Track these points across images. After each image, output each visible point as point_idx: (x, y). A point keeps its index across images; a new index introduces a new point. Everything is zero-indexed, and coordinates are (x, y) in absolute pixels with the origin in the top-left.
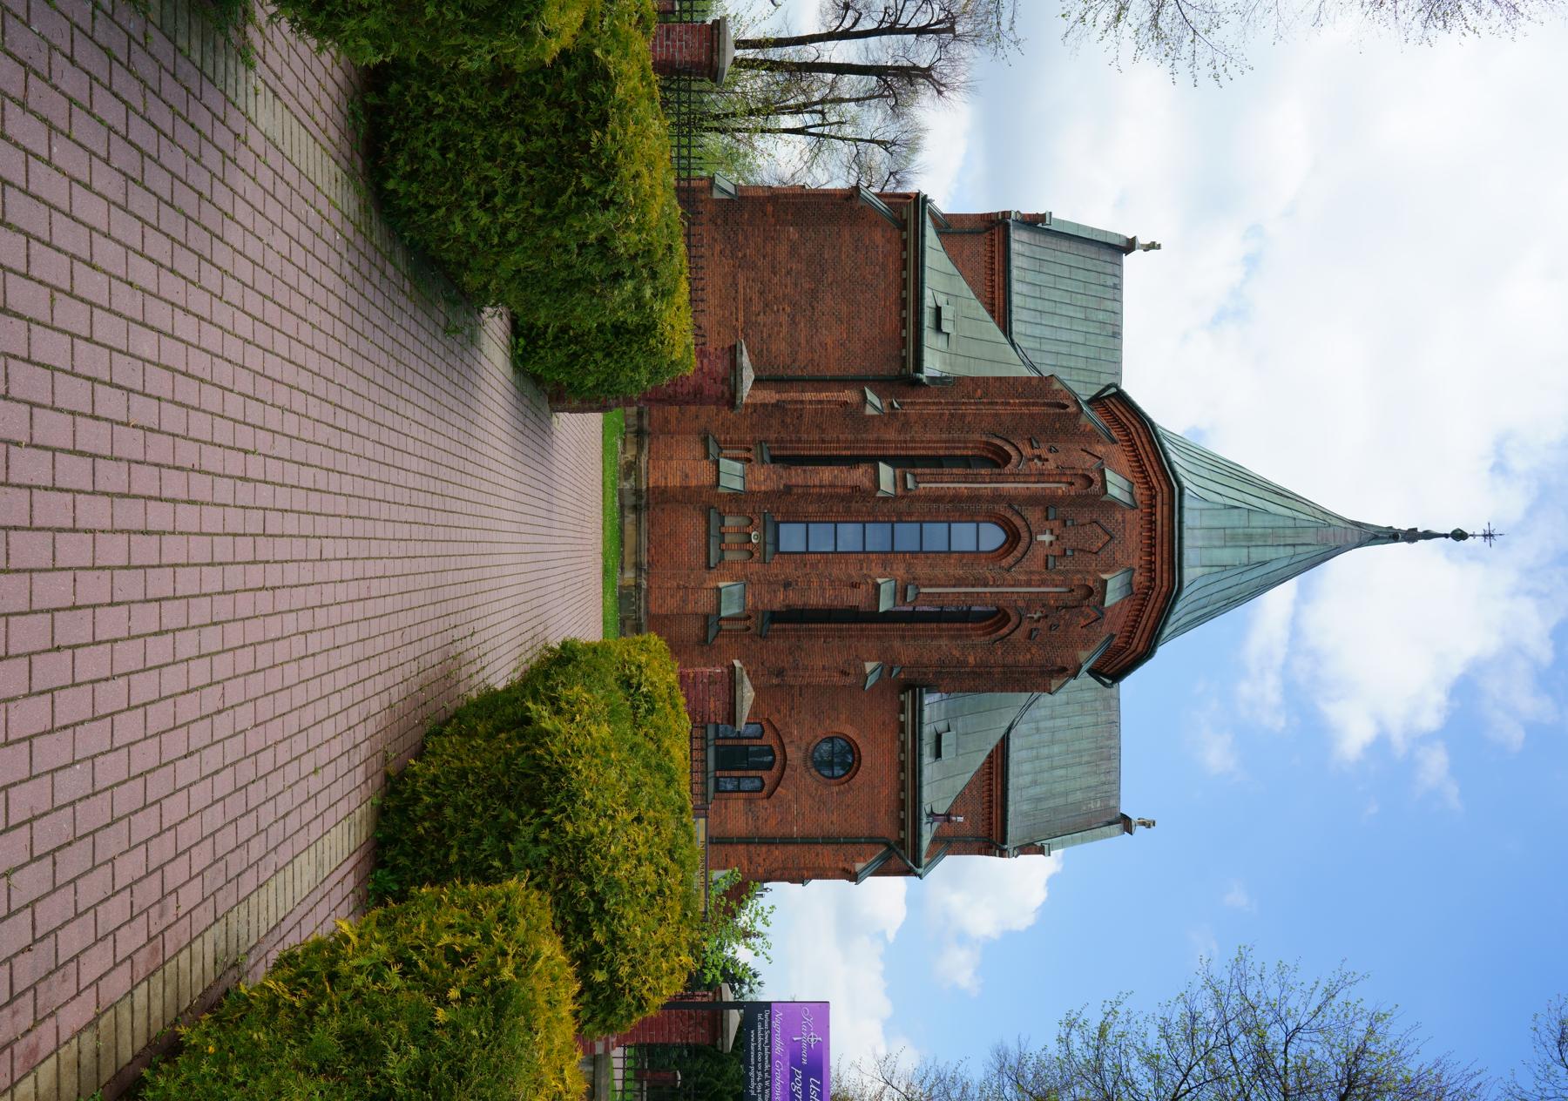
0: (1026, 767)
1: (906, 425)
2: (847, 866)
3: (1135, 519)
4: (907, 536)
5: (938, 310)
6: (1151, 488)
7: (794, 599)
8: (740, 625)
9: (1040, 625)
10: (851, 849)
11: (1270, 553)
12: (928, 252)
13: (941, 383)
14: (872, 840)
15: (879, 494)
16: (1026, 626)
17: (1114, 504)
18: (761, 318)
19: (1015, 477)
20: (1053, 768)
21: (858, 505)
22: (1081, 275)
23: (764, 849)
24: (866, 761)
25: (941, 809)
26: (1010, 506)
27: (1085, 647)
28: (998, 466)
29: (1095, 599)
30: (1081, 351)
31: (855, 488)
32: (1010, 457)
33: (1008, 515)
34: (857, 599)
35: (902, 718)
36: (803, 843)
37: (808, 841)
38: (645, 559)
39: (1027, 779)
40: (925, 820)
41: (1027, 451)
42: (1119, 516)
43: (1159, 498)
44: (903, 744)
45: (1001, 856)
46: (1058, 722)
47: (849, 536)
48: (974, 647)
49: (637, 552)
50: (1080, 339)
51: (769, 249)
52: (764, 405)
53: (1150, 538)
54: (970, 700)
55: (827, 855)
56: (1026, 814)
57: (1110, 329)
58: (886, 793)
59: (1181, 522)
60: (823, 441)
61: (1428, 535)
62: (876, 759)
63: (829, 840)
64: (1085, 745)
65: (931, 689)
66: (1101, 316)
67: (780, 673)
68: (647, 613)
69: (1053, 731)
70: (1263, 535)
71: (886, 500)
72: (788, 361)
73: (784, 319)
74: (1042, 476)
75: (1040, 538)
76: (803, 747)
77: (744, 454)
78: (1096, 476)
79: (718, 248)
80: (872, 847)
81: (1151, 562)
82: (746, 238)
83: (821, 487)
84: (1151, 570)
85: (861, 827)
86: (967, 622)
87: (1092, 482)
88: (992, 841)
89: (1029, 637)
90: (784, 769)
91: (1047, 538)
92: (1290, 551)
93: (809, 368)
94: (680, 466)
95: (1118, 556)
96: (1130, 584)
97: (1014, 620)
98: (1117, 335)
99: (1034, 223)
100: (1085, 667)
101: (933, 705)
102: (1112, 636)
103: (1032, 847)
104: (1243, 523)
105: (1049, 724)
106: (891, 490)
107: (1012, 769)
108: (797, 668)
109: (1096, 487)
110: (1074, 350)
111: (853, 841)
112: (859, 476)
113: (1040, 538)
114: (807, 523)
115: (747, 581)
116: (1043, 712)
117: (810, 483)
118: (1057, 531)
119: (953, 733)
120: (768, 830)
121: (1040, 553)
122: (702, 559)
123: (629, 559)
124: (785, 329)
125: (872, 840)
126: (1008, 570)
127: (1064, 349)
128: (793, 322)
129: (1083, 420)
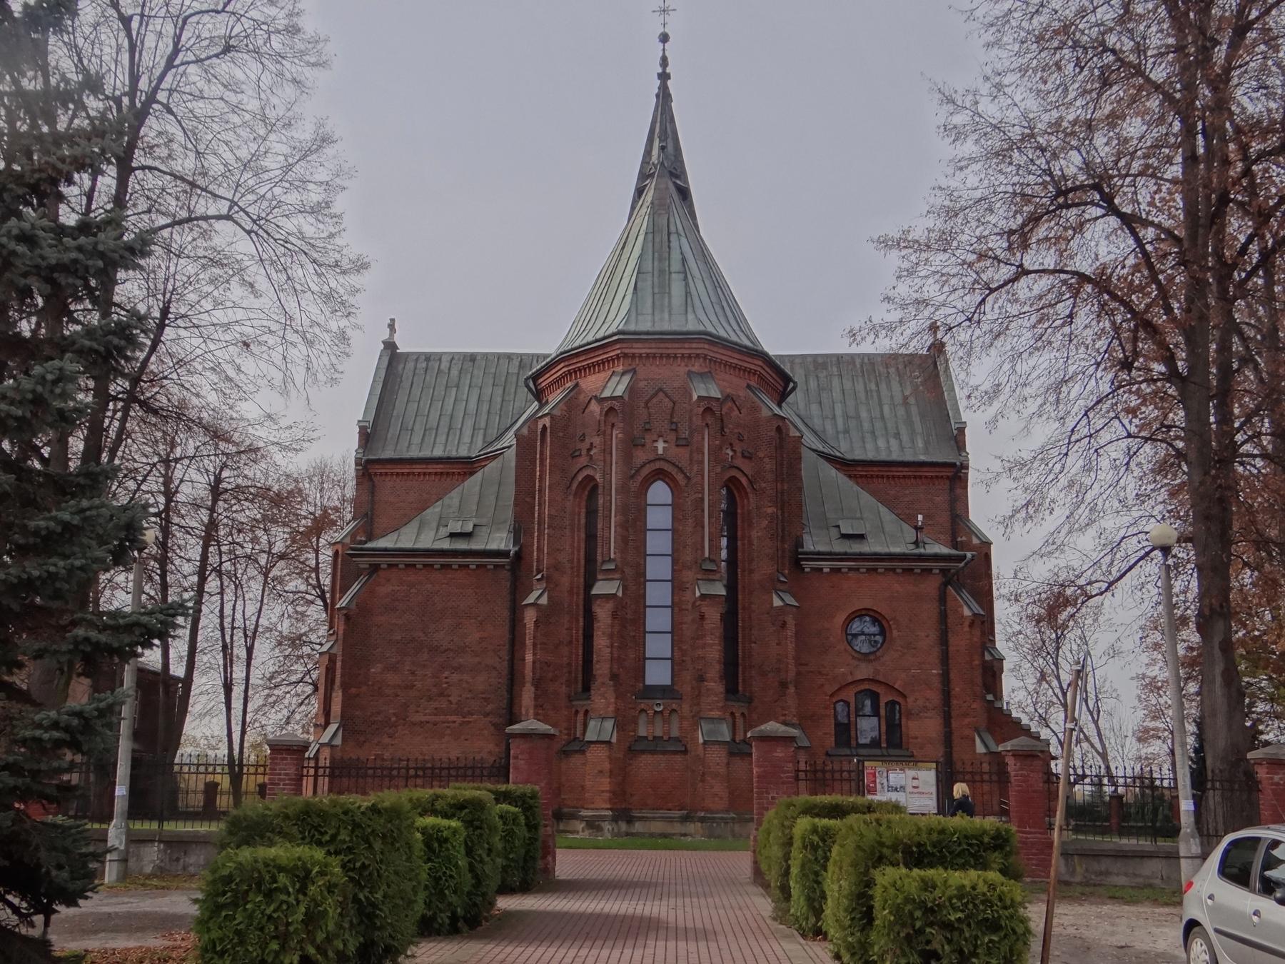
0: (881, 443)
1: (556, 567)
2: (967, 623)
3: (645, 370)
4: (659, 568)
5: (453, 535)
6: (618, 357)
7: (714, 671)
8: (740, 722)
9: (739, 450)
10: (951, 619)
11: (676, 256)
12: (400, 545)
13: (520, 531)
14: (943, 598)
15: (620, 594)
16: (739, 462)
17: (631, 389)
19: (606, 474)
20: (883, 417)
21: (631, 614)
22: (416, 391)
23: (954, 702)
24: (867, 603)
25: (910, 534)
26: (632, 477)
28: (596, 487)
29: (714, 405)
30: (487, 391)
31: (614, 615)
32: (588, 476)
33: (640, 479)
34: (714, 615)
36: (948, 665)
38: (677, 813)
39: (893, 442)
40: (922, 550)
41: (583, 460)
42: (642, 384)
43: (626, 351)
44: (850, 569)
45: (967, 468)
46: (838, 412)
47: (658, 620)
48: (758, 508)
49: (670, 820)
50: (476, 392)
52: (536, 698)
54: (810, 506)
55: (960, 641)
56: (927, 443)
57: (468, 365)
59: (647, 333)
60: (571, 642)
61: (664, 62)
62: (870, 592)
63: (944, 640)
64: (860, 387)
65: (799, 543)
66: (455, 373)
67: (784, 685)
68: (727, 811)
69: (847, 417)
70: (660, 260)
71: (625, 588)
73: (455, 677)
74: (607, 451)
75: (660, 451)
76: (856, 663)
77: (580, 717)
78: (607, 405)
79: (387, 740)
80: (949, 599)
82: (379, 713)
83: (612, 646)
84: (690, 357)
85: (929, 610)
86: (736, 513)
87: (612, 408)
88: (953, 476)
89: (750, 458)
91: (660, 446)
92: (674, 238)
94: (593, 775)
95: (676, 384)
96: (701, 375)
97: (734, 473)
98: (472, 358)
99: (367, 437)
100: (777, 410)
101: (812, 543)
102: (749, 386)
103: (958, 440)
105: (840, 421)
106: (617, 583)
107: (883, 456)
108: (779, 670)
109: (616, 405)
110: (486, 398)
111: (943, 617)
112: (603, 613)
113: (660, 451)
114: (645, 659)
115: (697, 718)
116: (829, 427)
117: (608, 656)
118: (655, 437)
119: (840, 523)
120: (935, 697)
122: (678, 758)
123: (678, 828)
125: (943, 598)
126: (689, 478)
127: (485, 407)
128: (458, 669)
129: (556, 412)
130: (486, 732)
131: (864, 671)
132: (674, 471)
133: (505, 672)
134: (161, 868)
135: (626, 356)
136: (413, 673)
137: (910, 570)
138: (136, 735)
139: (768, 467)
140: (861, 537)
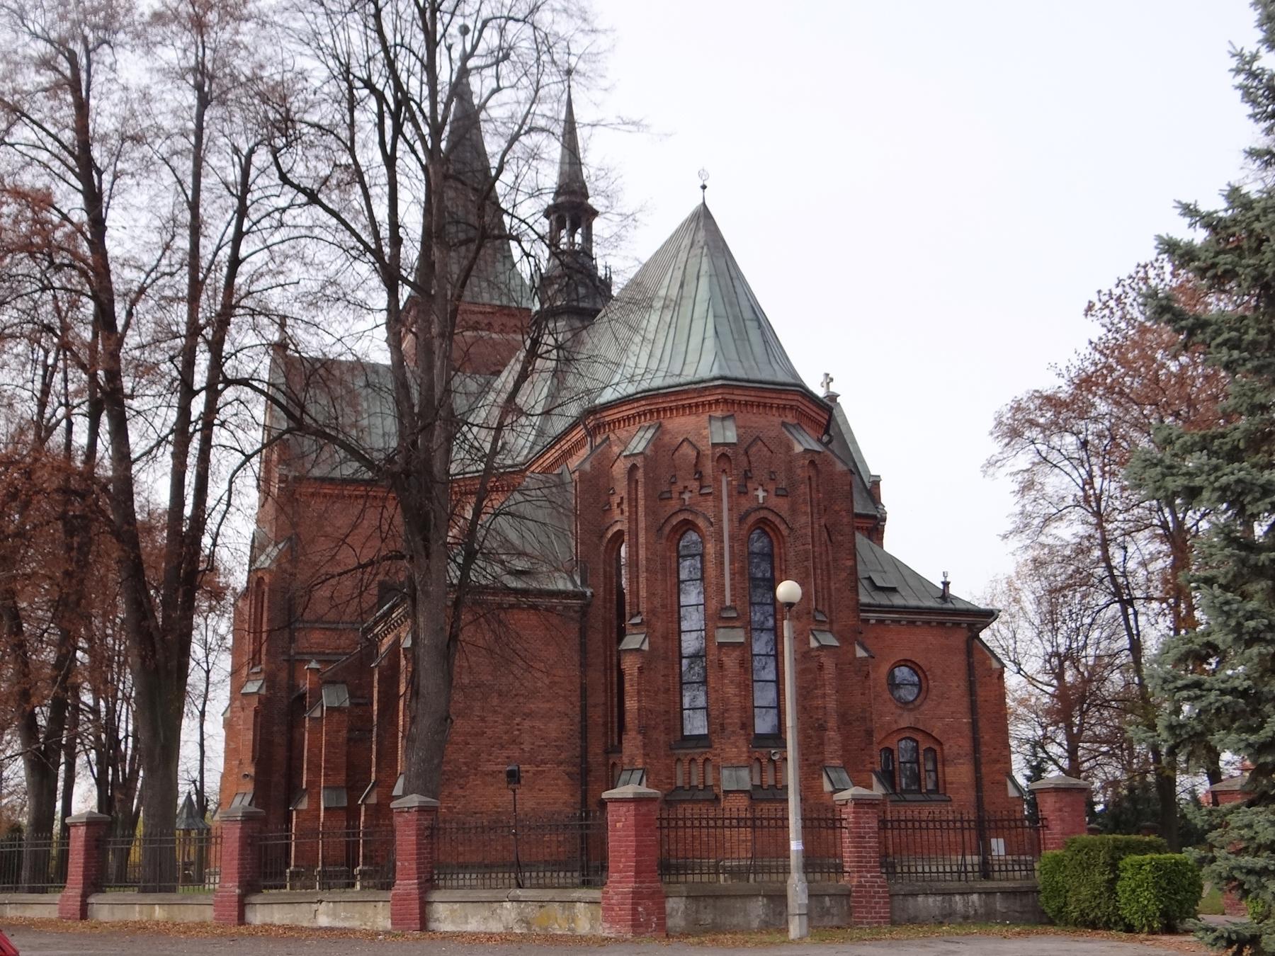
18: (527, 747)
24: (907, 655)
27: (789, 448)
35: (873, 621)
37: (973, 709)
44: (893, 621)
45: (884, 520)
48: (835, 560)
51: (460, 739)
53: (758, 406)
58: (932, 639)
70: (731, 304)
72: (566, 721)
73: (527, 724)
76: (899, 711)
78: (719, 451)
79: (458, 792)
81: (778, 407)
84: (784, 407)
90: (918, 730)
91: (761, 494)
93: (573, 699)
95: (773, 434)
102: (784, 424)
104: (725, 321)
109: (729, 451)
118: (756, 485)
120: (966, 745)
121: (774, 502)
124: (537, 724)
126: (791, 529)
128: (528, 715)
130: (560, 782)
131: (906, 720)
132: (777, 521)
133: (578, 719)
134: (766, 922)
135: (726, 401)
136: (483, 719)
137: (913, 622)
138: (56, 789)
139: (845, 520)
140: (894, 590)
